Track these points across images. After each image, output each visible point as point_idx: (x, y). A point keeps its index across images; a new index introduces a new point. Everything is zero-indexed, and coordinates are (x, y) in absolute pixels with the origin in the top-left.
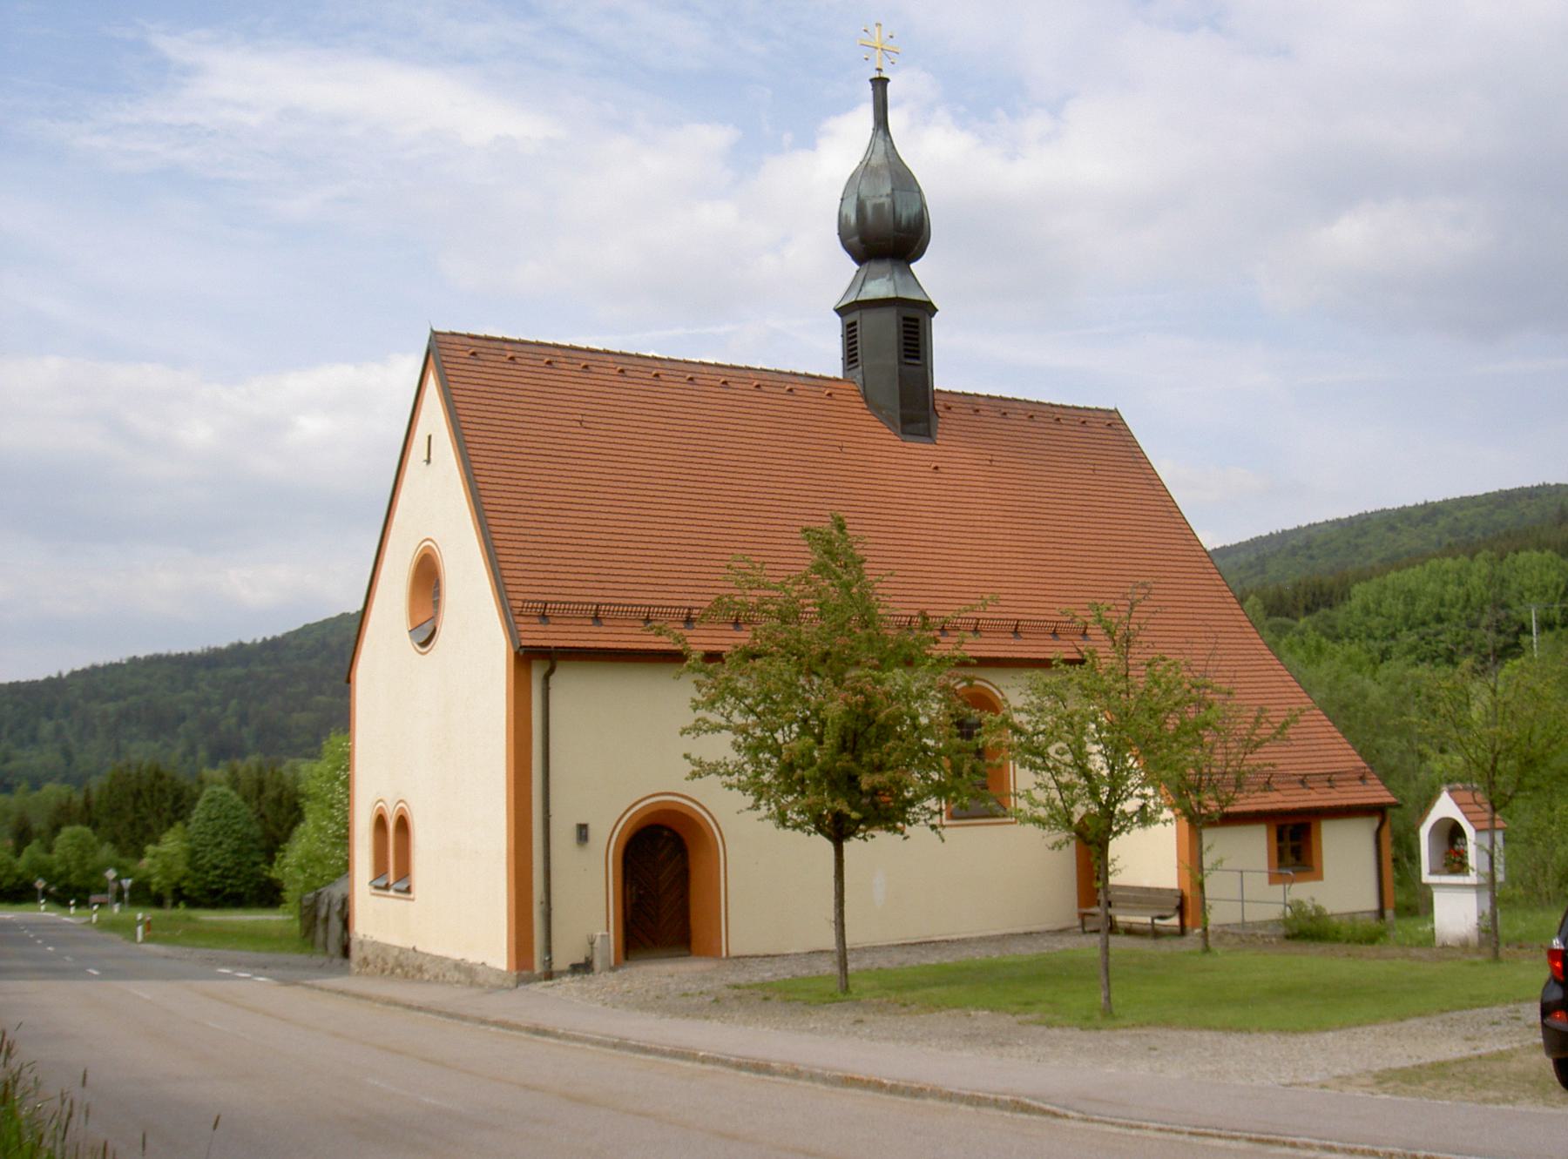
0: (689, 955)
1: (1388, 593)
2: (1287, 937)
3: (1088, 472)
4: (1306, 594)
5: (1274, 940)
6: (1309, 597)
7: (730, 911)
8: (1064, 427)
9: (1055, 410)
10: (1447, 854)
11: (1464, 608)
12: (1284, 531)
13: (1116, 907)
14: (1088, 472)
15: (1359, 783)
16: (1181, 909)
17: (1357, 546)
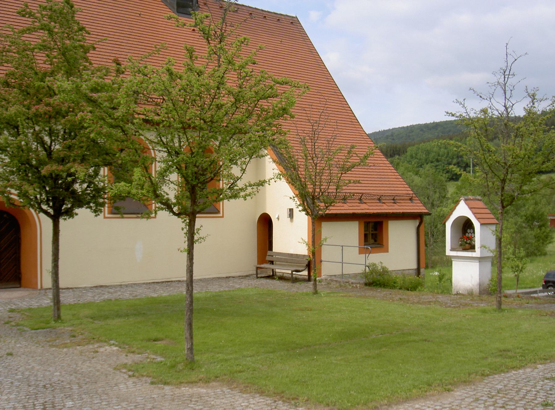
0: (20, 287)
1: (420, 151)
2: (366, 284)
3: (278, 42)
4: (391, 150)
5: (358, 285)
6: (392, 152)
7: (43, 262)
8: (268, 21)
9: (264, 13)
10: (461, 238)
11: (447, 157)
12: (384, 130)
13: (276, 264)
14: (278, 42)
15: (409, 202)
16: (309, 266)
17: (409, 136)
